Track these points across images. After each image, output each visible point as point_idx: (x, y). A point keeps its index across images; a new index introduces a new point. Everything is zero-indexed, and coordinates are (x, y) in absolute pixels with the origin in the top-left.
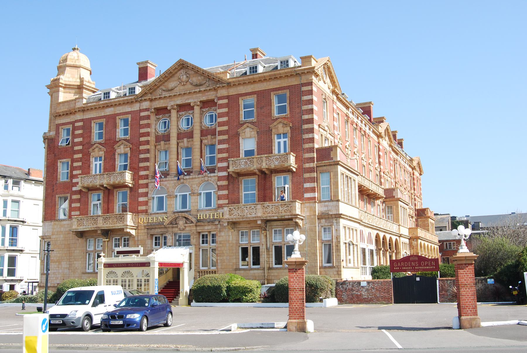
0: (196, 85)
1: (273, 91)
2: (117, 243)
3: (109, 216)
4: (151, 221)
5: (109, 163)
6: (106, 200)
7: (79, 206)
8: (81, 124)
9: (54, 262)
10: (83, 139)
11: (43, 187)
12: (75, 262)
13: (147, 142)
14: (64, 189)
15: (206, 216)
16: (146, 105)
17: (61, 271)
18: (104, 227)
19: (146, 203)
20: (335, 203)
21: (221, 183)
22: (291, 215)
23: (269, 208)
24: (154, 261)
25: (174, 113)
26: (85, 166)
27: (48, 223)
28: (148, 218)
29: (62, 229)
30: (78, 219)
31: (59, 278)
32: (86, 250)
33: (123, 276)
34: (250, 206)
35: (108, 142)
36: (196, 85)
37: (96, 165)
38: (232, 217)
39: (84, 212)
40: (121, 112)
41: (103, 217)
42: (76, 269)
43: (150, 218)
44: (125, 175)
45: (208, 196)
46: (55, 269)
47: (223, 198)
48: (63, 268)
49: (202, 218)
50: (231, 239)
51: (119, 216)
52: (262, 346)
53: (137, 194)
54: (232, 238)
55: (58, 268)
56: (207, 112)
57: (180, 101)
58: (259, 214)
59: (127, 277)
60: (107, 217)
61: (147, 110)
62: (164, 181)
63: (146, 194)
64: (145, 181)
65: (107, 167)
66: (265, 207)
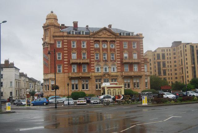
0: (109, 36)
8: (66, 41)
13: (117, 51)
16: (92, 39)
19: (94, 69)
21: (93, 65)
25: (101, 42)
33: (113, 90)
36: (109, 36)
37: (73, 56)
38: (125, 75)
45: (114, 68)
56: (111, 44)
57: (103, 39)
58: (133, 74)
61: (92, 40)
63: (94, 67)
64: (93, 63)
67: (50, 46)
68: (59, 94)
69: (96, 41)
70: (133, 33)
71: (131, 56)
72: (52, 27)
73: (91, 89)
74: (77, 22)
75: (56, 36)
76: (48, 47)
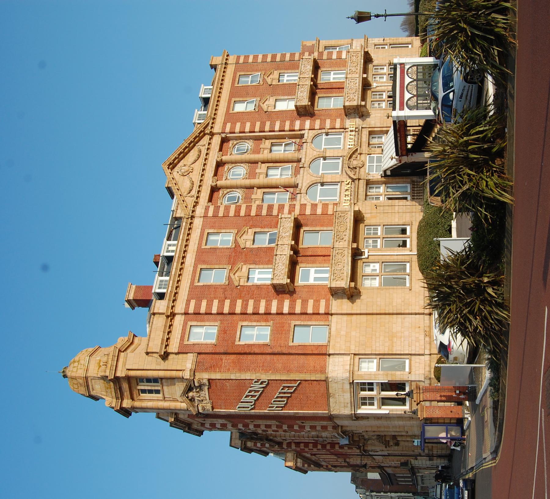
0: (199, 157)
2: (372, 232)
3: (336, 233)
5: (261, 258)
7: (312, 300)
9: (392, 346)
10: (215, 298)
11: (267, 341)
12: (394, 304)
14: (282, 334)
17: (406, 333)
18: (349, 234)
26: (256, 294)
28: (344, 201)
29: (343, 333)
30: (333, 279)
31: (417, 335)
35: (232, 260)
36: (199, 157)
39: (323, 293)
40: (197, 243)
41: (335, 241)
42: (404, 301)
46: (402, 343)
47: (334, 123)
48: (403, 329)
50: (379, 115)
51: (337, 219)
53: (312, 217)
54: (379, 113)
55: (402, 338)
58: (357, 76)
60: (336, 235)
62: (302, 185)
65: (267, 260)
66: (337, 239)
67: (206, 370)
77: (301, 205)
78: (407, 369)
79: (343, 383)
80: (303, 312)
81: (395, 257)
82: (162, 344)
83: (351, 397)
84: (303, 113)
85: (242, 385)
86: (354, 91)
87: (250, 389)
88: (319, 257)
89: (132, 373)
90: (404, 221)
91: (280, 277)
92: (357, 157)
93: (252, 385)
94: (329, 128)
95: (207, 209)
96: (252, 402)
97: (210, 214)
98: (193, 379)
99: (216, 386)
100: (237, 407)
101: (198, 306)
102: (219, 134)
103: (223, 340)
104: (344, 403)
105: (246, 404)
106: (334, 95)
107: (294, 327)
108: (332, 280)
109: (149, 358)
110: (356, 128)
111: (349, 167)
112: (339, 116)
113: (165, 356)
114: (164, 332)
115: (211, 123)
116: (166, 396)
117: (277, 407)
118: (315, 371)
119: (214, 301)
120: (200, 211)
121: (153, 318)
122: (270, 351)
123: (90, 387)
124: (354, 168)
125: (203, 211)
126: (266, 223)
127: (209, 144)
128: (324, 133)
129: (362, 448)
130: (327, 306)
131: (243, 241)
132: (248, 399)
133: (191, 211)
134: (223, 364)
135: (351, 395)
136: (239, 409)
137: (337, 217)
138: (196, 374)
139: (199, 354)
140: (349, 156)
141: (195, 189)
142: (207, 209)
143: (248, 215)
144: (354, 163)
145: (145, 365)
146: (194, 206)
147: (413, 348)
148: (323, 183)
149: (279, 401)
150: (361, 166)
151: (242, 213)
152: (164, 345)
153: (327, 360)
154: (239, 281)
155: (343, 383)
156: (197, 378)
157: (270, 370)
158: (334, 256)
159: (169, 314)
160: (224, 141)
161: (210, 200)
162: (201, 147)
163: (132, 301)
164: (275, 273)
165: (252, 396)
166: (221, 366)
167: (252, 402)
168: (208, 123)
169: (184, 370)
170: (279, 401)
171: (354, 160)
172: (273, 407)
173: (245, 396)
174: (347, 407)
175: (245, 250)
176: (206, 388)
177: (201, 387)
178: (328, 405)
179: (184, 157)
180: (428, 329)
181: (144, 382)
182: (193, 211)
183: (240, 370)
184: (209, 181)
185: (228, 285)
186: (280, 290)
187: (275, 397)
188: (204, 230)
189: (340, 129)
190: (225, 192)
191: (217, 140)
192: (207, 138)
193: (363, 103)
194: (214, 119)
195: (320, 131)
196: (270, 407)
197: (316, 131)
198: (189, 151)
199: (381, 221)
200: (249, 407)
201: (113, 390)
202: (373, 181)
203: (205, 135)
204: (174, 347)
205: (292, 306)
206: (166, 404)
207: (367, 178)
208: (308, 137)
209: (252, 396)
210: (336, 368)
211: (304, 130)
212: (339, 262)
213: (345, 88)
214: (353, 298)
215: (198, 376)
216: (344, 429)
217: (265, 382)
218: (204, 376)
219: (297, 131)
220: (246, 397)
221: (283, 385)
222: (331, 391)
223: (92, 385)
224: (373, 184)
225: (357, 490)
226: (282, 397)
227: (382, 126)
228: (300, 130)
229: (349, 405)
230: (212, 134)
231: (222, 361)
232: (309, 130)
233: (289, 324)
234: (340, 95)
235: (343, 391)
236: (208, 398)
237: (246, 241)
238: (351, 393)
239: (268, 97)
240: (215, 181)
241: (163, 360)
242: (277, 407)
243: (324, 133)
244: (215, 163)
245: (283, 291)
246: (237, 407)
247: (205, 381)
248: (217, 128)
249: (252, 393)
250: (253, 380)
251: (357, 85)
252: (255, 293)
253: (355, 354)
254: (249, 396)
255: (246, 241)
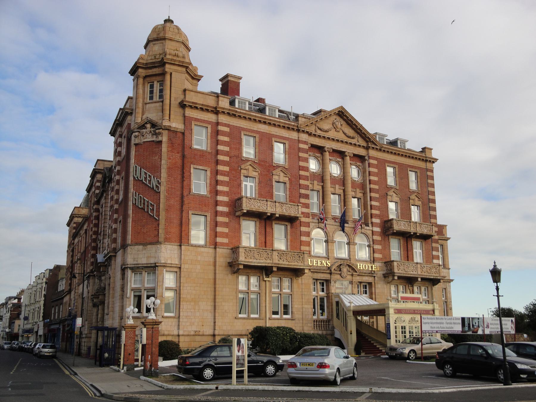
0: (349, 137)
1: (195, 121)
3: (285, 252)
4: (316, 264)
6: (263, 232)
10: (230, 148)
14: (200, 205)
15: (365, 267)
20: (447, 270)
22: (272, 264)
23: (283, 256)
24: (388, 308)
27: (171, 246)
29: (199, 258)
32: (237, 288)
34: (412, 264)
36: (349, 137)
40: (277, 134)
41: (278, 252)
43: (314, 260)
44: (393, 223)
46: (189, 310)
49: (361, 269)
50: (386, 292)
51: (297, 254)
52: (291, 398)
55: (193, 310)
58: (419, 273)
59: (414, 324)
65: (262, 193)
66: (280, 254)
67: (170, 139)
68: (194, 328)
69: (314, 147)
70: (404, 142)
71: (406, 214)
72: (180, 69)
73: (301, 316)
74: (240, 78)
75: (194, 107)
76: (161, 142)
77: (309, 223)
78: (166, 314)
79: (155, 257)
80: (218, 223)
81: (264, 305)
82: (193, 103)
83: (143, 264)
84: (386, 225)
85: (156, 169)
86: (406, 270)
87: (152, 176)
88: (264, 238)
89: (168, 77)
90: (295, 313)
91: (248, 204)
92: (349, 271)
93: (155, 178)
94: (374, 247)
95: (305, 143)
96: (140, 177)
97: (302, 146)
98: (162, 128)
99: (155, 148)
100: (137, 165)
101: (224, 134)
102: (368, 154)
103: (195, 155)
104: (138, 258)
105: (139, 173)
106: (402, 253)
107: (205, 216)
108: (245, 249)
109: (180, 92)
110: (374, 271)
111: (341, 265)
112: (384, 257)
113: (182, 105)
114: (202, 105)
115: (377, 147)
116: (147, 105)
117: (135, 199)
118: (167, 233)
119: (228, 148)
120: (304, 137)
121: (214, 96)
122: (185, 194)
123: (156, 42)
124: (340, 269)
125: (304, 140)
126: (294, 193)
127: (359, 146)
128: (370, 243)
129: (92, 274)
130: (222, 244)
131: (278, 173)
132: (143, 175)
133: (304, 130)
134: (174, 154)
135: (144, 264)
136: (135, 167)
137: (299, 254)
138: (167, 131)
139: (183, 134)
140: (350, 265)
141: (322, 134)
142: (305, 143)
143: (300, 177)
144: (345, 270)
145: (175, 88)
146: (307, 132)
147: (185, 320)
148: (328, 242)
149: (141, 201)
150: (342, 276)
151: (302, 173)
152: (191, 105)
153: (176, 244)
154: (245, 169)
155: (155, 257)
156: (163, 132)
157: (168, 194)
158: (266, 251)
159: (218, 109)
160: (361, 158)
161: (313, 146)
162: (356, 139)
163: (227, 79)
164: (252, 199)
165: (146, 178)
166: (173, 152)
167: (140, 177)
168: (376, 145)
169: (170, 121)
170: (141, 201)
171: (347, 269)
172: (136, 196)
173: (146, 172)
174: (134, 260)
175: (271, 174)
176: (154, 139)
177: (156, 134)
178: (137, 244)
179: (348, 124)
180: (201, 333)
181: (160, 87)
182: (303, 131)
183: (169, 169)
184: (329, 145)
185: (242, 160)
186: (237, 204)
187: (144, 198)
188: (288, 140)
189: (374, 258)
190: (319, 159)
191: (362, 152)
192: (363, 143)
193: (396, 278)
194: (380, 150)
195: (371, 240)
196: (136, 193)
197: (371, 237)
198: (353, 129)
199: (295, 293)
200: (136, 175)
201: (154, 61)
202: (329, 285)
203: (367, 142)
204: (189, 112)
205: (223, 214)
206: (140, 105)
207: (332, 281)
208: (366, 229)
209: (146, 178)
210: (169, 252)
211: (372, 227)
212: (261, 255)
213: (408, 262)
214: (229, 268)
215: (165, 133)
216: (113, 258)
217: (158, 190)
218: (164, 138)
219: (371, 220)
220: (145, 172)
221: (155, 205)
222: (149, 246)
223: (157, 44)
224: (326, 286)
225: (48, 270)
226: (144, 204)
227: (376, 294)
228: (372, 223)
229: (135, 262)
230: (367, 148)
231: (177, 153)
232: (372, 231)
233: (207, 211)
234: (403, 258)
235: (148, 257)
236: (145, 140)
237: (279, 176)
238: (147, 264)
239: (399, 196)
240: (329, 150)
241: (179, 103)
242: (135, 199)
243: (370, 243)
244: (343, 150)
245: (236, 207)
246: (137, 165)
247: (160, 138)
248: (372, 153)
249: (148, 178)
250: (160, 179)
251: (412, 273)
252: (234, 182)
253: (180, 268)
254: (146, 176)
255: (279, 176)
